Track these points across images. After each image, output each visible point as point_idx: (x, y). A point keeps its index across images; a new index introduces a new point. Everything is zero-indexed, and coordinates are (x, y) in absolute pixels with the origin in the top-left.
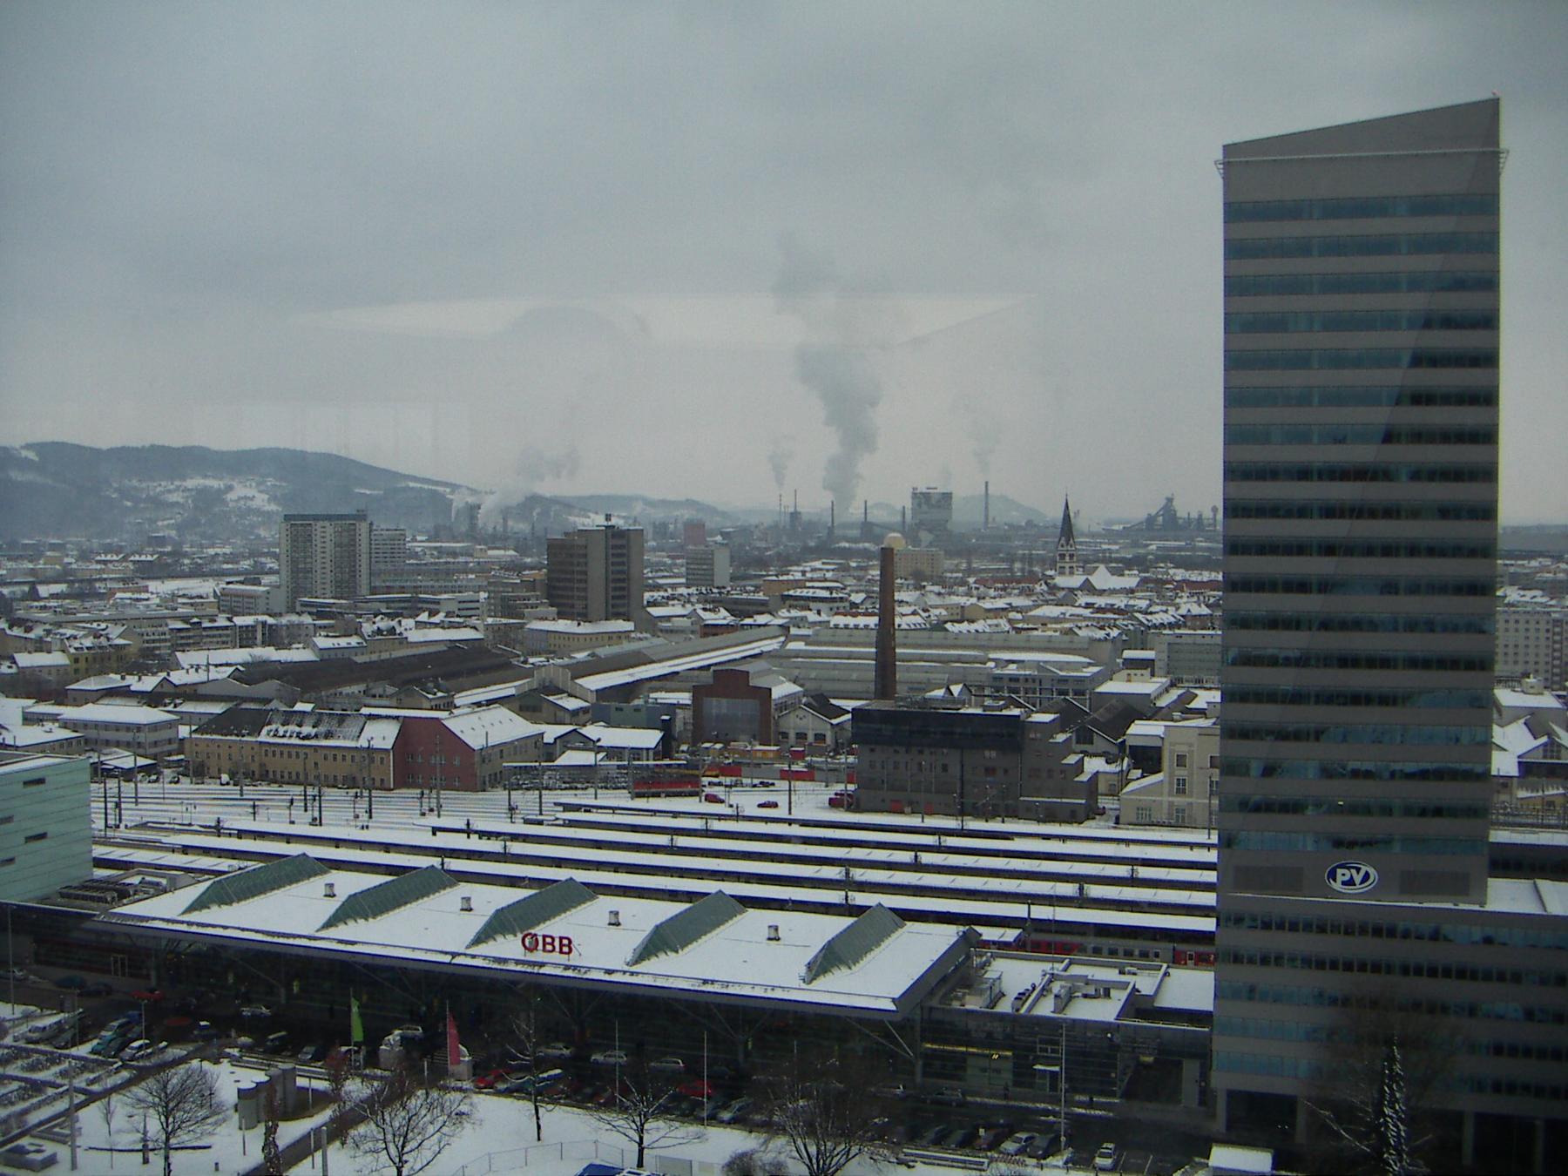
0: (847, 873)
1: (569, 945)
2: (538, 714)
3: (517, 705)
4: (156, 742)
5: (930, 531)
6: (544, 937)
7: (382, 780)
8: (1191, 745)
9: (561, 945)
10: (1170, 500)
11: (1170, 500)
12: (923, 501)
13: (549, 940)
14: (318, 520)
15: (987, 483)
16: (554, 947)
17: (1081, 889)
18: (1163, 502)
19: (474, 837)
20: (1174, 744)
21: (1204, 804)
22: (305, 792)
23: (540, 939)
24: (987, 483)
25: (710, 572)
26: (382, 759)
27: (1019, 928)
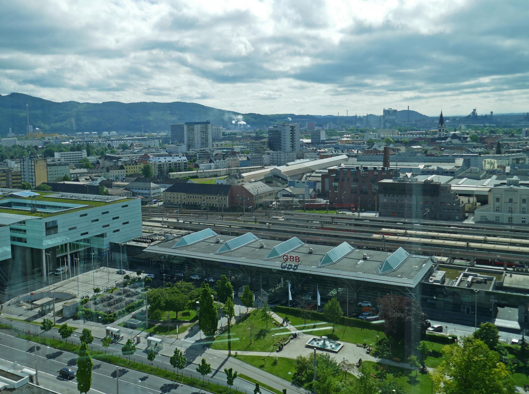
0: (383, 237)
1: (299, 259)
2: (272, 184)
3: (265, 181)
4: (154, 193)
5: (389, 123)
6: (290, 256)
7: (225, 205)
8: (502, 194)
9: (296, 259)
10: (475, 110)
11: (475, 110)
12: (387, 113)
13: (292, 257)
14: (439, 138)
15: (408, 106)
16: (294, 260)
17: (468, 244)
18: (472, 111)
19: (257, 224)
20: (521, 195)
21: (514, 213)
22: (359, 215)
23: (289, 257)
24: (408, 106)
25: (319, 138)
26: (225, 198)
27: (447, 257)
